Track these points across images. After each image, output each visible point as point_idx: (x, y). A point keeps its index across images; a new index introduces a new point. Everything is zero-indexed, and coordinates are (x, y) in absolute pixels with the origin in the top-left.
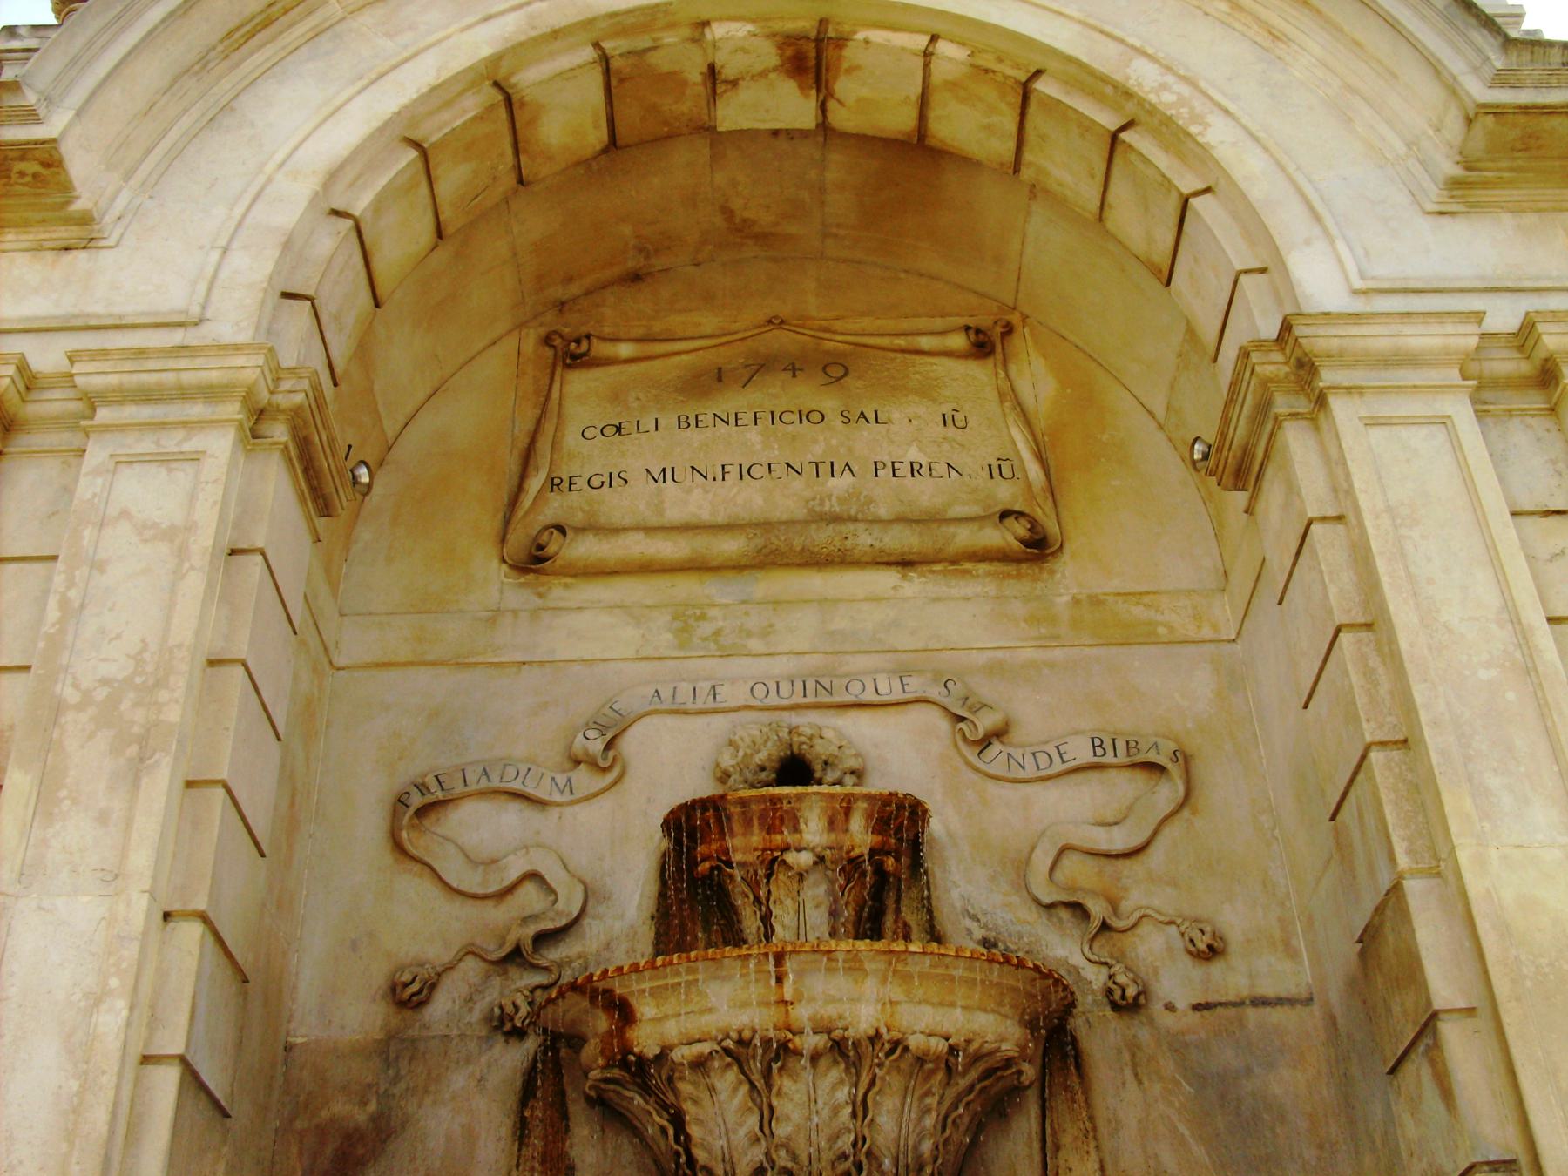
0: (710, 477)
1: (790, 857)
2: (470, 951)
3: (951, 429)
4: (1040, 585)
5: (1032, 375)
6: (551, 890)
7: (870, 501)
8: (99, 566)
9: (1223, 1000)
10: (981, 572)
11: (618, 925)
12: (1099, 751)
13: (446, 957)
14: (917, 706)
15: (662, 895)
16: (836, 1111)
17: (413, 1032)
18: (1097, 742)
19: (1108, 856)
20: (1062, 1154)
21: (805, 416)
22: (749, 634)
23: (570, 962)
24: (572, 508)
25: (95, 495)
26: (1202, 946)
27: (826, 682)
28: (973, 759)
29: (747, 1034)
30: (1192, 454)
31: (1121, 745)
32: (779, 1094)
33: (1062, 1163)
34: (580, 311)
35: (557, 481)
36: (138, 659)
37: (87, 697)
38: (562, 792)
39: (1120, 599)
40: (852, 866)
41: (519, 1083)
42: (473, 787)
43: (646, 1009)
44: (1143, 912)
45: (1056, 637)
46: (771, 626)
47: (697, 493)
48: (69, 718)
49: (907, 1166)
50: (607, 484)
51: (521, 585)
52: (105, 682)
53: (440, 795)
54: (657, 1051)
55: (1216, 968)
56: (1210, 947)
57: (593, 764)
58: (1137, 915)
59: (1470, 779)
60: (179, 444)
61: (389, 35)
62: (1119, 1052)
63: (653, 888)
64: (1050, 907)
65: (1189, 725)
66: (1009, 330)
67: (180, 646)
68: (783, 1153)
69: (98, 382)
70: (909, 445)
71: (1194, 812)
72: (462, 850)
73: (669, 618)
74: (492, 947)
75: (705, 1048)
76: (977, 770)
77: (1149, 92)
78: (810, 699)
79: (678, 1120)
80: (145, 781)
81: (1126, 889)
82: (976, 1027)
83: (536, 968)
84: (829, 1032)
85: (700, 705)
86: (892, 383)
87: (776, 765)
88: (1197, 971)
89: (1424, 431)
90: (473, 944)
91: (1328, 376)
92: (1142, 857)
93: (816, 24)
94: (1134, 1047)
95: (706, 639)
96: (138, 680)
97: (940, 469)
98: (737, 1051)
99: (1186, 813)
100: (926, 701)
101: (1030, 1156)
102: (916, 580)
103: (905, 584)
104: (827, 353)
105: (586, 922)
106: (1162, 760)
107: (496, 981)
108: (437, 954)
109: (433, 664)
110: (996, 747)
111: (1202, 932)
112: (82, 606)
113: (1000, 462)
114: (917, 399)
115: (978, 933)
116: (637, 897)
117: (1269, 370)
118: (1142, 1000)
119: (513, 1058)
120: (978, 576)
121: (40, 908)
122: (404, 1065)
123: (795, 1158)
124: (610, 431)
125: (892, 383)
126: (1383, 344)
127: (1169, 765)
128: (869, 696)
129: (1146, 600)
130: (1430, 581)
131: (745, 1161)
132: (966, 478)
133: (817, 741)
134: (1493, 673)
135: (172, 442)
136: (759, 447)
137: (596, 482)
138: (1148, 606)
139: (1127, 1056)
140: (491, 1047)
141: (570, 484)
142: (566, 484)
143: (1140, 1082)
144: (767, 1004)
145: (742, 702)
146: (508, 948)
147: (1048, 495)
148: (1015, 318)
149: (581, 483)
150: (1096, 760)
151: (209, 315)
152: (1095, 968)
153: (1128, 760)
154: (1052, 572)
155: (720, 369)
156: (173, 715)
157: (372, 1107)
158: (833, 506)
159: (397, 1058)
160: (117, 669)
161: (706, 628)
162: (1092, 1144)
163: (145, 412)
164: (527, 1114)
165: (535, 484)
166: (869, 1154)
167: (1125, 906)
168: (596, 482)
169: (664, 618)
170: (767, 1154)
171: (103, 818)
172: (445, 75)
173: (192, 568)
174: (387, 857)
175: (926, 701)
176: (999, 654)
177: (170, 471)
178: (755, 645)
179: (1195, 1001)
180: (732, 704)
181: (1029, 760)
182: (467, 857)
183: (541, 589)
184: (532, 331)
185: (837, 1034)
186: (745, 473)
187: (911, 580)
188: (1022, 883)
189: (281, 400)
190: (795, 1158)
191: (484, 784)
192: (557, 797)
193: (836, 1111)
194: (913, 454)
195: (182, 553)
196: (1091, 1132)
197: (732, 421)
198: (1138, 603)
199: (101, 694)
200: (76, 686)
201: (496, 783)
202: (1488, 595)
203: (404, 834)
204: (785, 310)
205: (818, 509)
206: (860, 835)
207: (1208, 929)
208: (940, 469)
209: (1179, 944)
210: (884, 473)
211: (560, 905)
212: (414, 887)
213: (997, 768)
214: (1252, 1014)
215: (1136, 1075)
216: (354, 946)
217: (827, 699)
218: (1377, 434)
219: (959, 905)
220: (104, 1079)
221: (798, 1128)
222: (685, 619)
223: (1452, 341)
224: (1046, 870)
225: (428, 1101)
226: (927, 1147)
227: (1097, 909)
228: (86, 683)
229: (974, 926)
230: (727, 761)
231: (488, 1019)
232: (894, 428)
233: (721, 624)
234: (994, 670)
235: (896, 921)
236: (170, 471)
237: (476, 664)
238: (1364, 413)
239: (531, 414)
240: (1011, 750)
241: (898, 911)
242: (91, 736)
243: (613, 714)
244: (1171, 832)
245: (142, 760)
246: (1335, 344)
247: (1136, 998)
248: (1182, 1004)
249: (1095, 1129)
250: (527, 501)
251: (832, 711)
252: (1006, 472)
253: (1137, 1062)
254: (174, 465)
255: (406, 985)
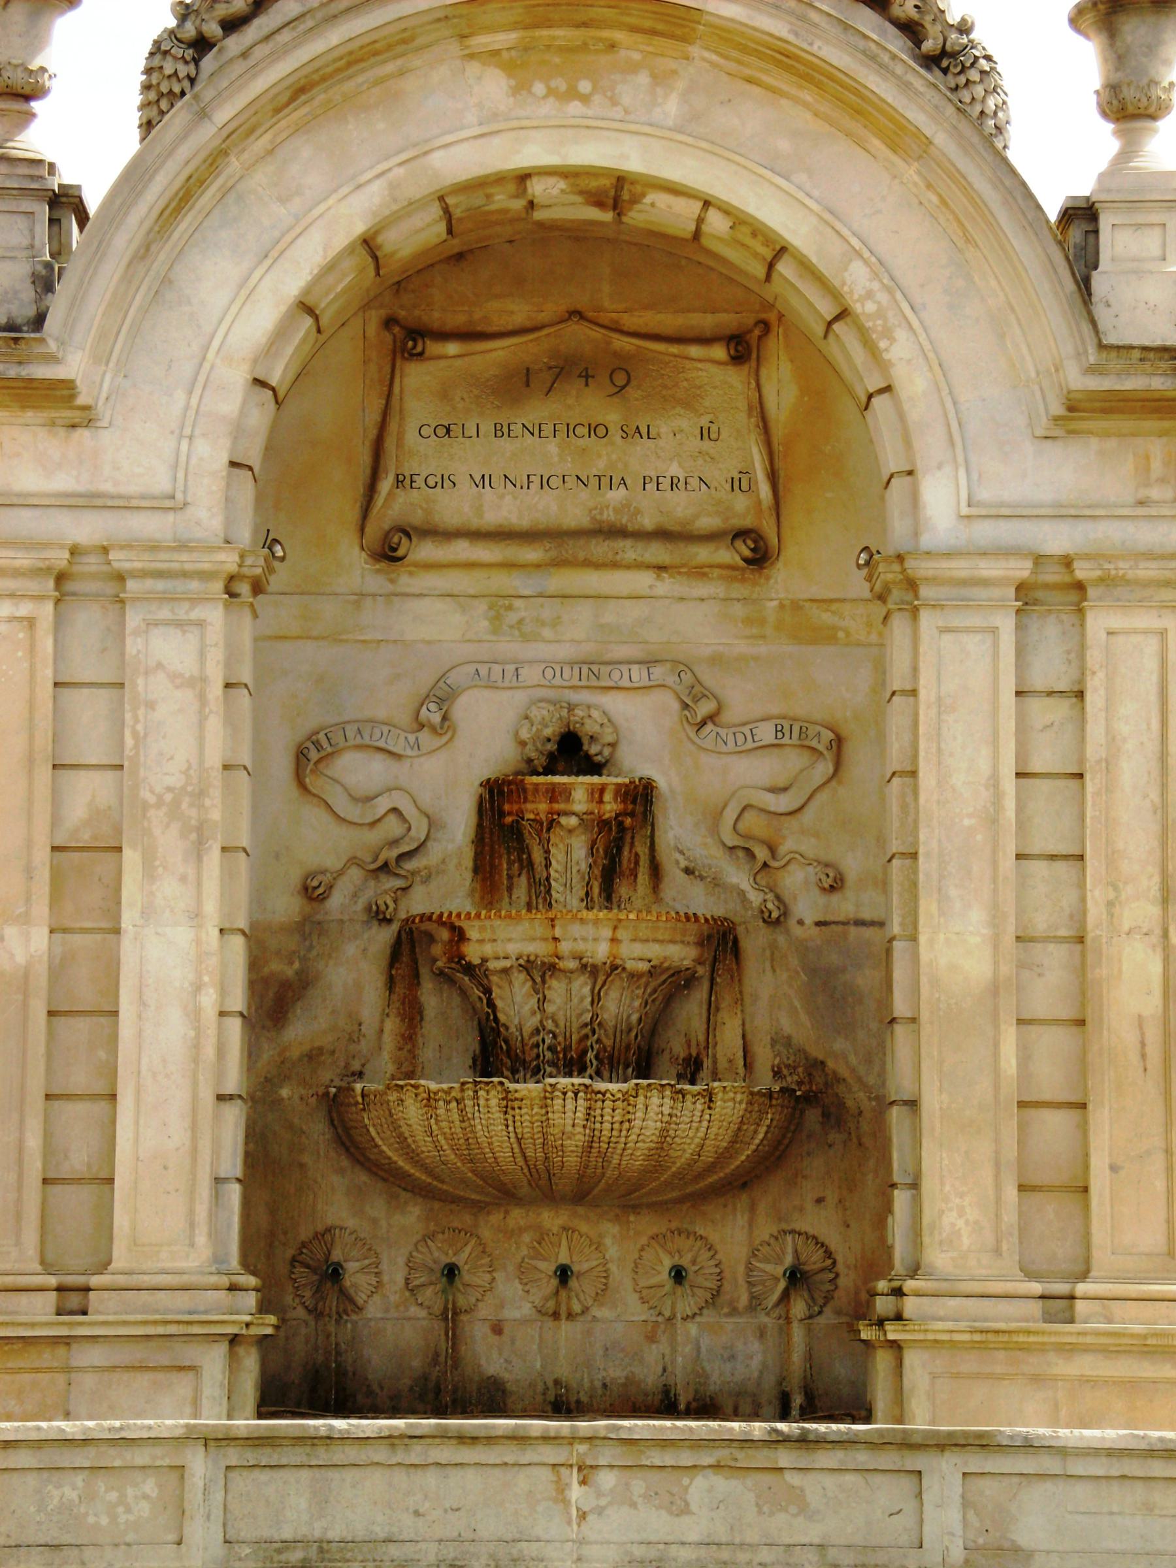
0: (518, 485)
1: (564, 820)
2: (354, 861)
3: (706, 442)
4: (757, 589)
5: (779, 381)
6: (405, 820)
7: (638, 512)
8: (151, 705)
9: (837, 919)
10: (715, 575)
11: (450, 846)
12: (780, 735)
13: (339, 866)
14: (657, 689)
15: (480, 826)
16: (582, 999)
17: (319, 917)
18: (779, 728)
19: (775, 814)
20: (720, 1015)
21: (593, 429)
22: (543, 624)
23: (419, 872)
24: (412, 504)
25: (139, 652)
26: (827, 886)
27: (595, 668)
28: (692, 735)
29: (532, 958)
30: (858, 560)
31: (796, 730)
32: (549, 988)
33: (719, 1019)
34: (413, 291)
35: (401, 478)
36: (186, 772)
37: (160, 798)
38: (412, 748)
39: (815, 605)
40: (603, 824)
41: (388, 952)
42: (351, 743)
43: (473, 933)
44: (792, 855)
45: (763, 637)
46: (559, 618)
47: (508, 498)
48: (152, 813)
49: (622, 1031)
50: (439, 484)
51: (378, 571)
52: (169, 789)
53: (329, 750)
54: (479, 961)
55: (835, 898)
56: (831, 886)
57: (433, 729)
58: (788, 858)
59: (940, 890)
60: (187, 613)
61: (283, 200)
62: (764, 950)
63: (473, 820)
64: (732, 848)
65: (848, 714)
66: (766, 326)
67: (212, 768)
68: (550, 1021)
69: (127, 565)
70: (671, 460)
71: (840, 782)
72: (346, 789)
73: (486, 607)
74: (369, 859)
75: (507, 964)
76: (693, 743)
77: (858, 301)
78: (584, 683)
79: (488, 991)
80: (205, 858)
81: (784, 838)
82: (668, 953)
83: (397, 875)
84: (581, 959)
85: (506, 684)
86: (664, 392)
87: (557, 738)
88: (822, 899)
89: (979, 637)
90: (355, 858)
91: (925, 592)
92: (798, 816)
93: (614, 181)
94: (773, 946)
95: (511, 627)
96: (190, 789)
97: (694, 482)
98: (528, 966)
99: (834, 783)
100: (664, 686)
101: (700, 1014)
102: (667, 581)
103: (658, 584)
104: (616, 354)
105: (429, 844)
106: (821, 747)
107: (372, 883)
108: (333, 863)
109: (316, 638)
110: (709, 727)
111: (828, 875)
112: (146, 735)
113: (741, 475)
114: (682, 412)
115: (683, 863)
116: (463, 827)
117: (890, 577)
118: (782, 919)
119: (384, 936)
120: (712, 579)
121: (157, 933)
122: (315, 937)
123: (557, 1026)
124: (441, 431)
125: (664, 392)
126: (963, 574)
127: (825, 752)
128: (625, 683)
129: (834, 607)
130: (951, 755)
131: (529, 1024)
132: (713, 491)
133: (587, 721)
134: (973, 821)
135: (182, 611)
136: (556, 459)
137: (431, 483)
138: (833, 613)
139: (768, 953)
140: (370, 928)
141: (412, 482)
142: (408, 481)
143: (774, 971)
144: (546, 940)
145: (535, 683)
146: (379, 863)
147: (773, 512)
148: (772, 317)
149: (419, 481)
150: (776, 742)
151: (189, 500)
152: (756, 893)
153: (798, 743)
154: (768, 578)
155: (528, 369)
156: (216, 815)
157: (297, 965)
158: (609, 516)
159: (310, 934)
160: (175, 780)
161: (512, 617)
162: (740, 1008)
163: (160, 585)
164: (393, 972)
165: (385, 485)
166: (600, 1024)
167: (782, 850)
168: (431, 483)
169: (482, 606)
170: (541, 1022)
171: (183, 879)
172: (331, 254)
173: (211, 712)
174: (294, 791)
175: (664, 686)
176: (721, 648)
177: (184, 632)
178: (547, 633)
179: (817, 920)
180: (529, 683)
181: (731, 738)
182: (350, 795)
183: (393, 576)
184: (373, 312)
185: (584, 961)
186: (544, 483)
187: (663, 580)
188: (714, 830)
189: (246, 571)
190: (557, 1026)
191: (359, 741)
192: (409, 752)
193: (582, 999)
194: (675, 470)
195: (202, 698)
196: (740, 1001)
197: (536, 432)
198: (827, 610)
199: (168, 797)
200: (152, 792)
201: (367, 741)
202: (984, 766)
203: (307, 780)
204: (582, 301)
205: (598, 517)
206: (610, 807)
207: (831, 875)
208: (694, 482)
209: (813, 879)
210: (651, 487)
211: (413, 833)
212: (314, 815)
213: (708, 743)
214: (853, 930)
215: (772, 967)
216: (277, 856)
217: (594, 683)
218: (947, 638)
219: (672, 843)
220: (209, 1032)
221: (559, 1009)
222: (500, 603)
223: (1011, 573)
224: (732, 823)
225: (331, 963)
226: (635, 1018)
227: (761, 854)
228: (158, 789)
229: (680, 858)
230: (525, 734)
231: (368, 909)
232: (661, 443)
233: (523, 614)
234: (716, 660)
235: (630, 852)
236: (184, 632)
237: (347, 641)
238: (940, 624)
239: (377, 404)
240: (719, 730)
241: (632, 844)
242: (168, 826)
243: (447, 688)
244: (823, 797)
245: (200, 843)
246: (930, 573)
247: (778, 919)
248: (809, 921)
249: (742, 1000)
250: (380, 500)
251: (599, 691)
252: (744, 486)
253: (774, 956)
254: (186, 628)
255: (315, 888)
